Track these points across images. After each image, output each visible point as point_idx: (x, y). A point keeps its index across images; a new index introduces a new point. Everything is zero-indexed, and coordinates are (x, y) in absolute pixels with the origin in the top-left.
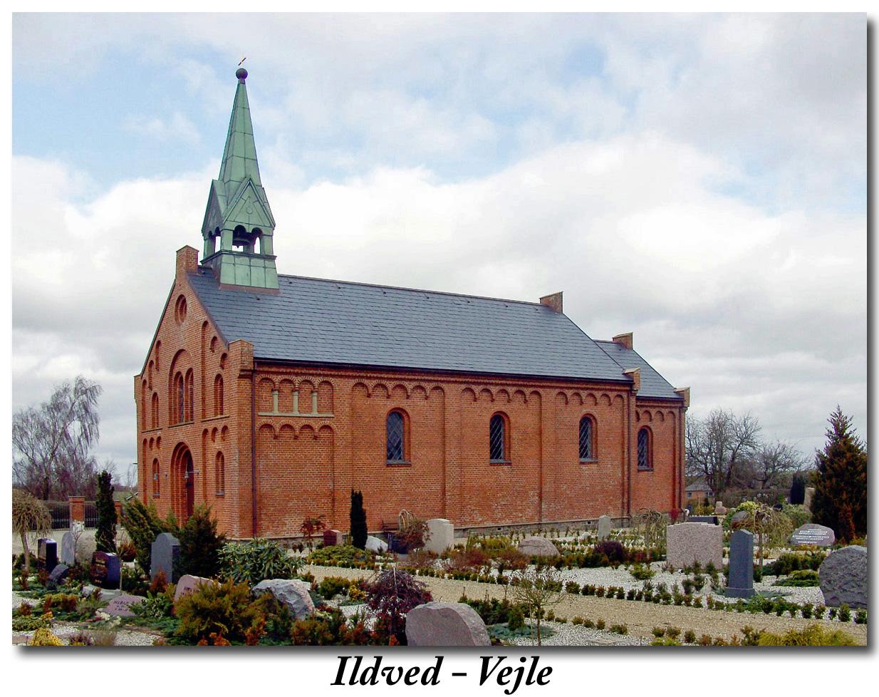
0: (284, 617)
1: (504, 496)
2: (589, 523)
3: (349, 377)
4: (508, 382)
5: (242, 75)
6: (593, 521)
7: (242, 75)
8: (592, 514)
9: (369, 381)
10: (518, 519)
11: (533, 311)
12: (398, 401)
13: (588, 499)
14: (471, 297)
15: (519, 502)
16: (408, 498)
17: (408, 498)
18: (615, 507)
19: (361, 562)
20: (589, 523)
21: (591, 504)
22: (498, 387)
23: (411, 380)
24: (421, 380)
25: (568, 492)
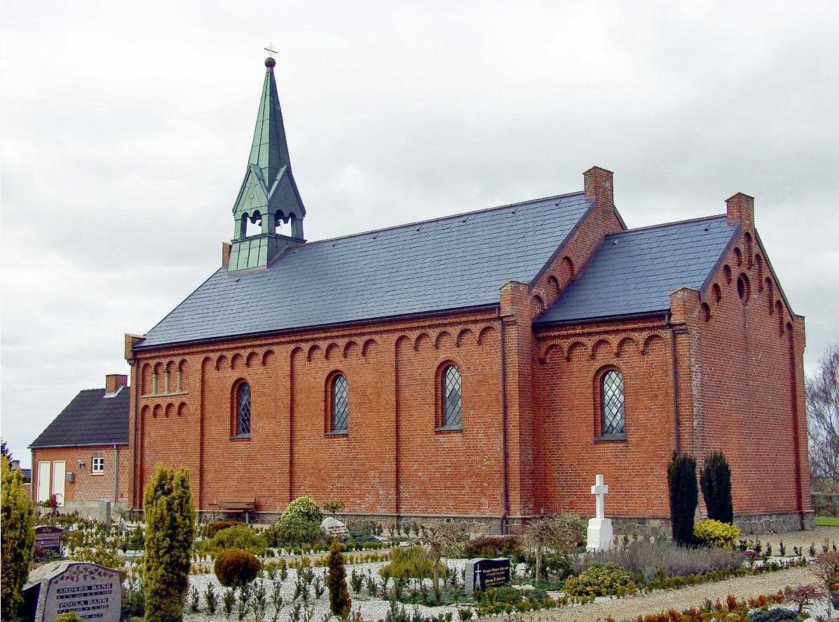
0: (345, 596)
1: (339, 477)
2: (448, 521)
3: (198, 352)
4: (333, 334)
5: (270, 64)
6: (454, 518)
7: (270, 64)
8: (456, 508)
9: (214, 354)
10: (356, 508)
11: (511, 215)
12: (241, 372)
13: (449, 484)
14: (420, 224)
15: (357, 485)
16: (247, 475)
17: (247, 475)
18: (492, 498)
19: (697, 577)
20: (448, 521)
21: (454, 492)
22: (644, 333)
23: (589, 334)
24: (208, 351)
25: (420, 474)
